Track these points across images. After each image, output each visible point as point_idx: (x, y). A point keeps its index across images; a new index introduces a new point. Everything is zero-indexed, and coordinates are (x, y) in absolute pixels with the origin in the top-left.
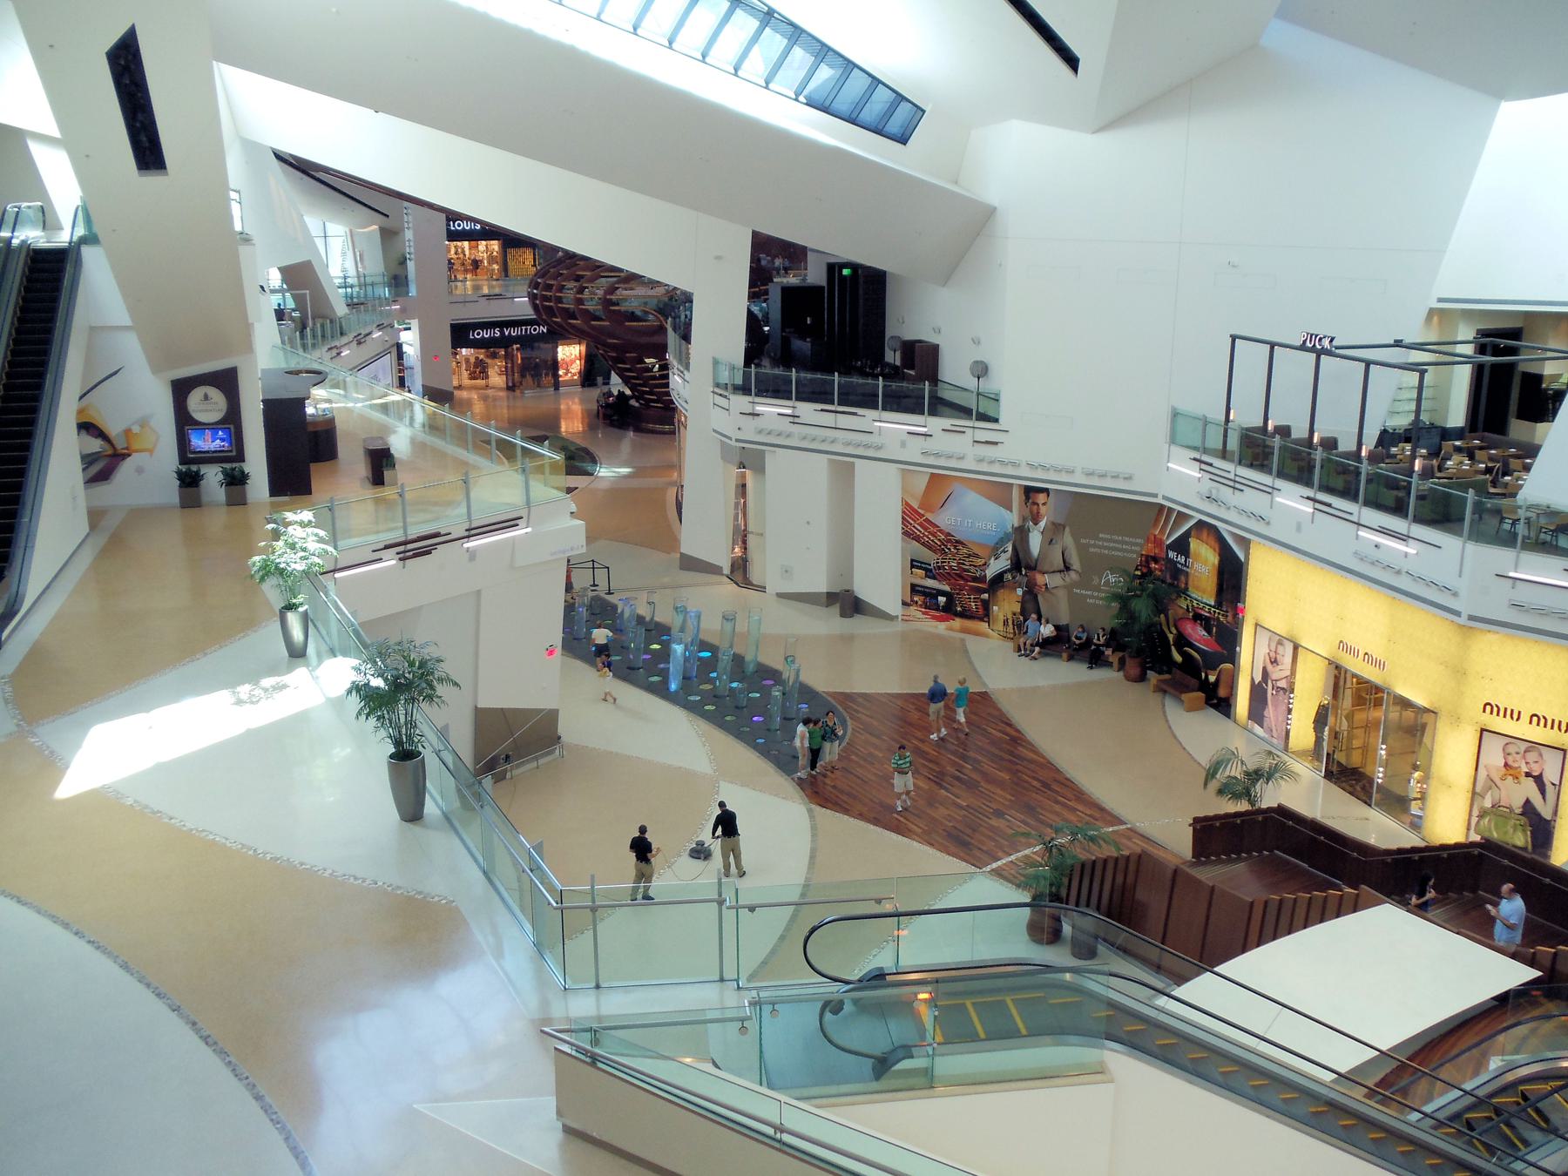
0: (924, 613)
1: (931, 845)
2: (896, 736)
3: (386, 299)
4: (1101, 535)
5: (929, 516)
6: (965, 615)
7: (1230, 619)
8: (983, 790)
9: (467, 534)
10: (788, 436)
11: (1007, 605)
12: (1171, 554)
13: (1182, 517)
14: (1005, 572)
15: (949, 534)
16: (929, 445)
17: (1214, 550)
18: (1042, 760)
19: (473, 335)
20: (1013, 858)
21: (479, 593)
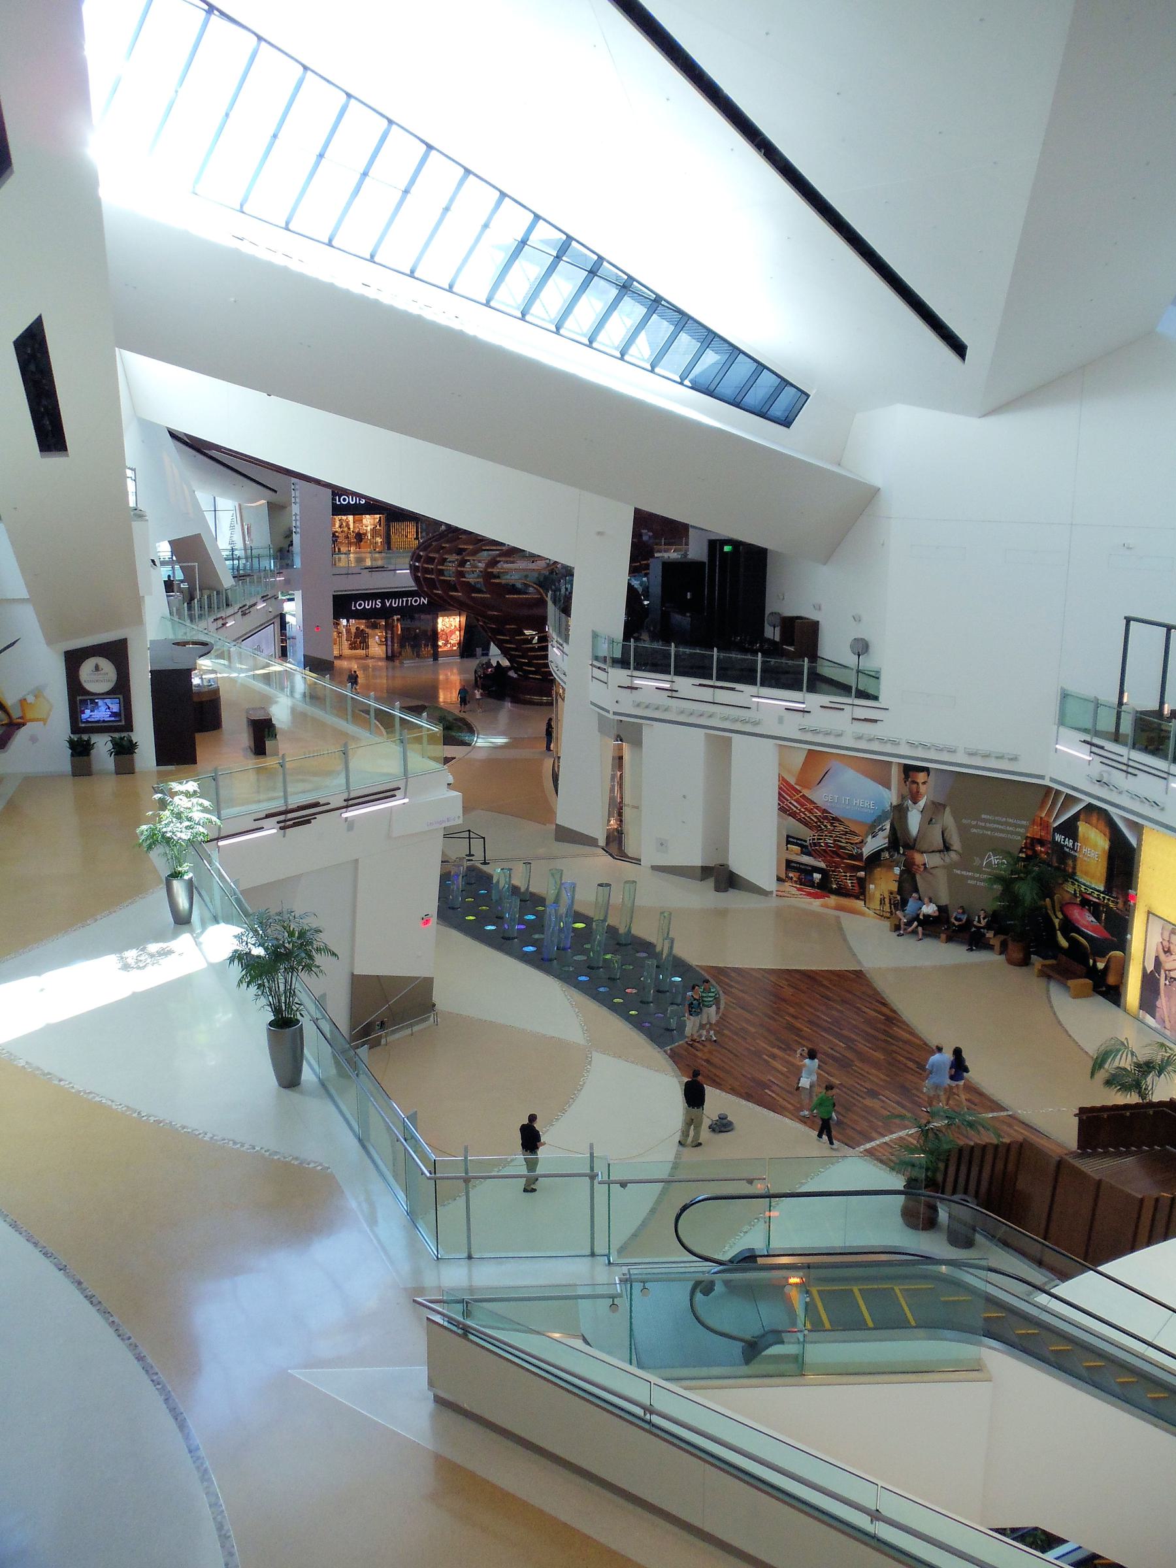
5: (806, 792)
6: (841, 892)
7: (1120, 905)
9: (345, 804)
10: (666, 710)
11: (884, 884)
14: (882, 850)
15: (825, 811)
16: (807, 721)
18: (916, 1040)
19: (339, 501)
20: (887, 1139)
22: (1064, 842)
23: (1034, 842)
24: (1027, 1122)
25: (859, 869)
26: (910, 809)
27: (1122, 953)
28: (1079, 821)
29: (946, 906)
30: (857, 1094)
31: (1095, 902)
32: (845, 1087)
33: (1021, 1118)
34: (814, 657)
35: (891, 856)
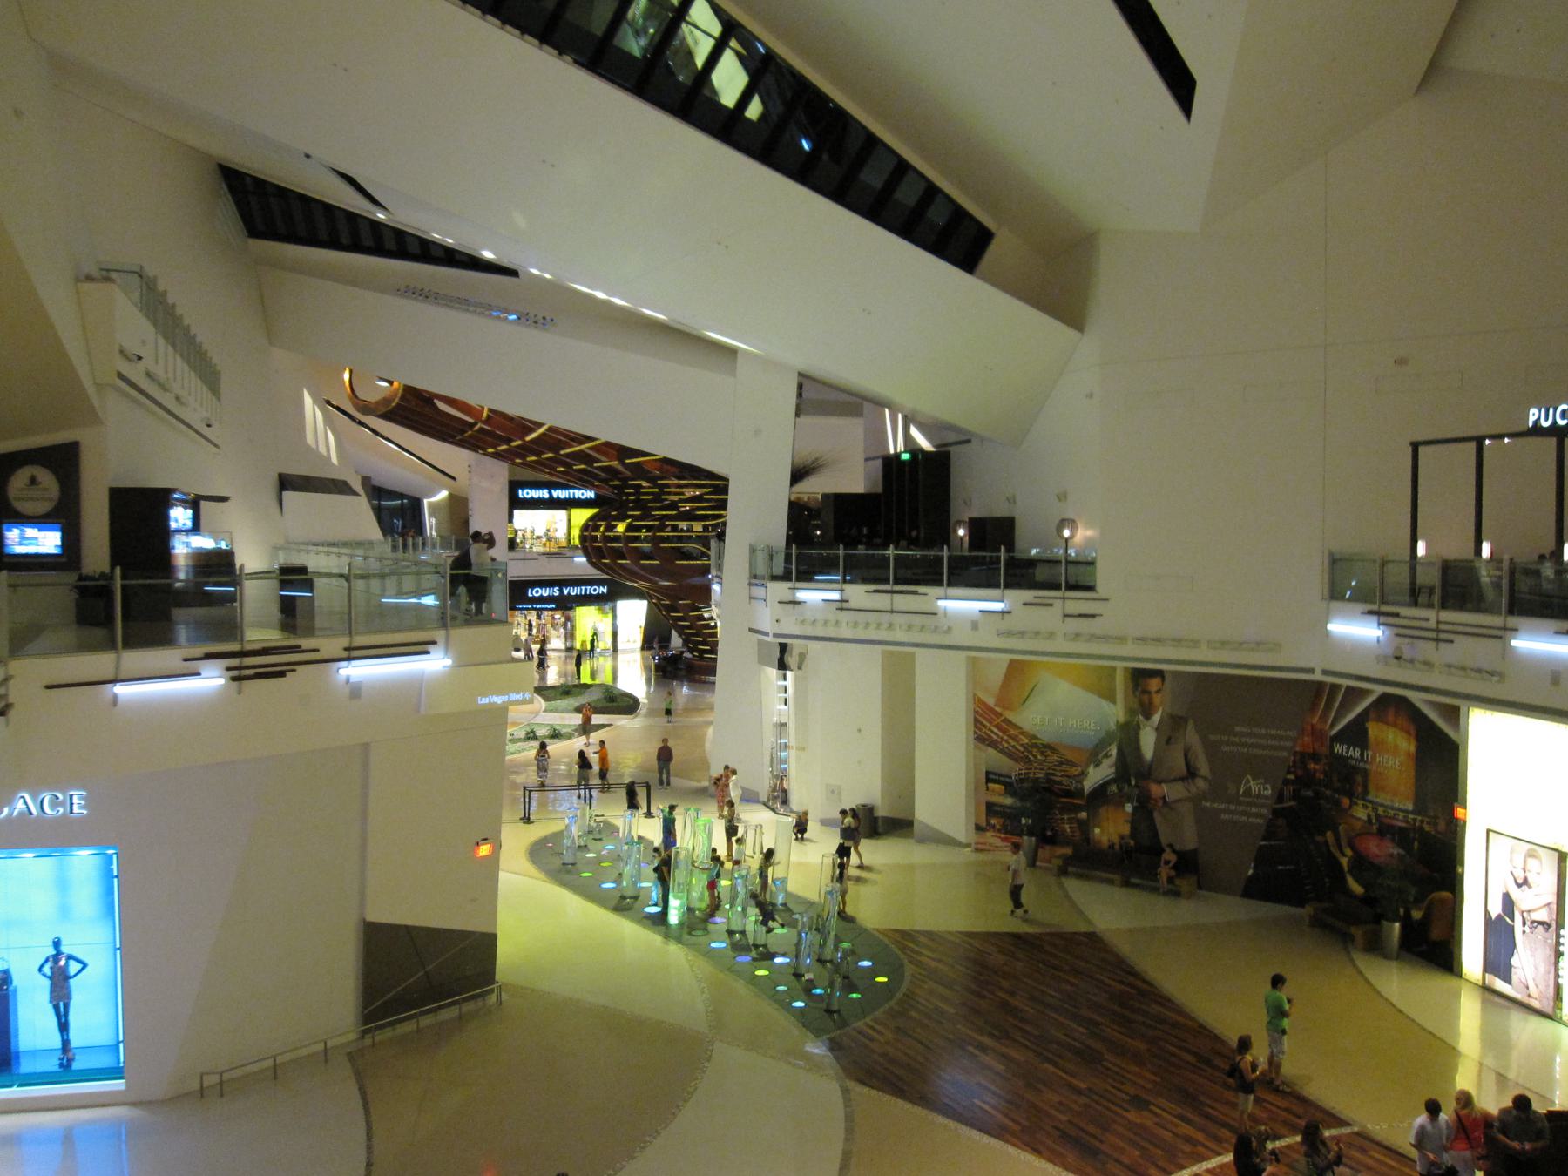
0: (1004, 840)
1: (1037, 1152)
2: (974, 987)
3: (432, 539)
4: (1238, 729)
5: (1011, 716)
8: (1110, 1066)
9: (345, 654)
12: (1338, 748)
13: (1359, 694)
15: (1034, 737)
17: (1408, 733)
18: (1190, 1023)
19: (532, 593)
21: (366, 747)
22: (1347, 752)
23: (1303, 758)
24: (1386, 1143)
25: (1079, 808)
26: (1142, 726)
27: (1451, 895)
28: (1367, 721)
29: (1195, 852)
30: (1113, 1103)
31: (1400, 828)
32: (1096, 1094)
33: (1379, 1138)
34: (1011, 547)
35: (1120, 790)
